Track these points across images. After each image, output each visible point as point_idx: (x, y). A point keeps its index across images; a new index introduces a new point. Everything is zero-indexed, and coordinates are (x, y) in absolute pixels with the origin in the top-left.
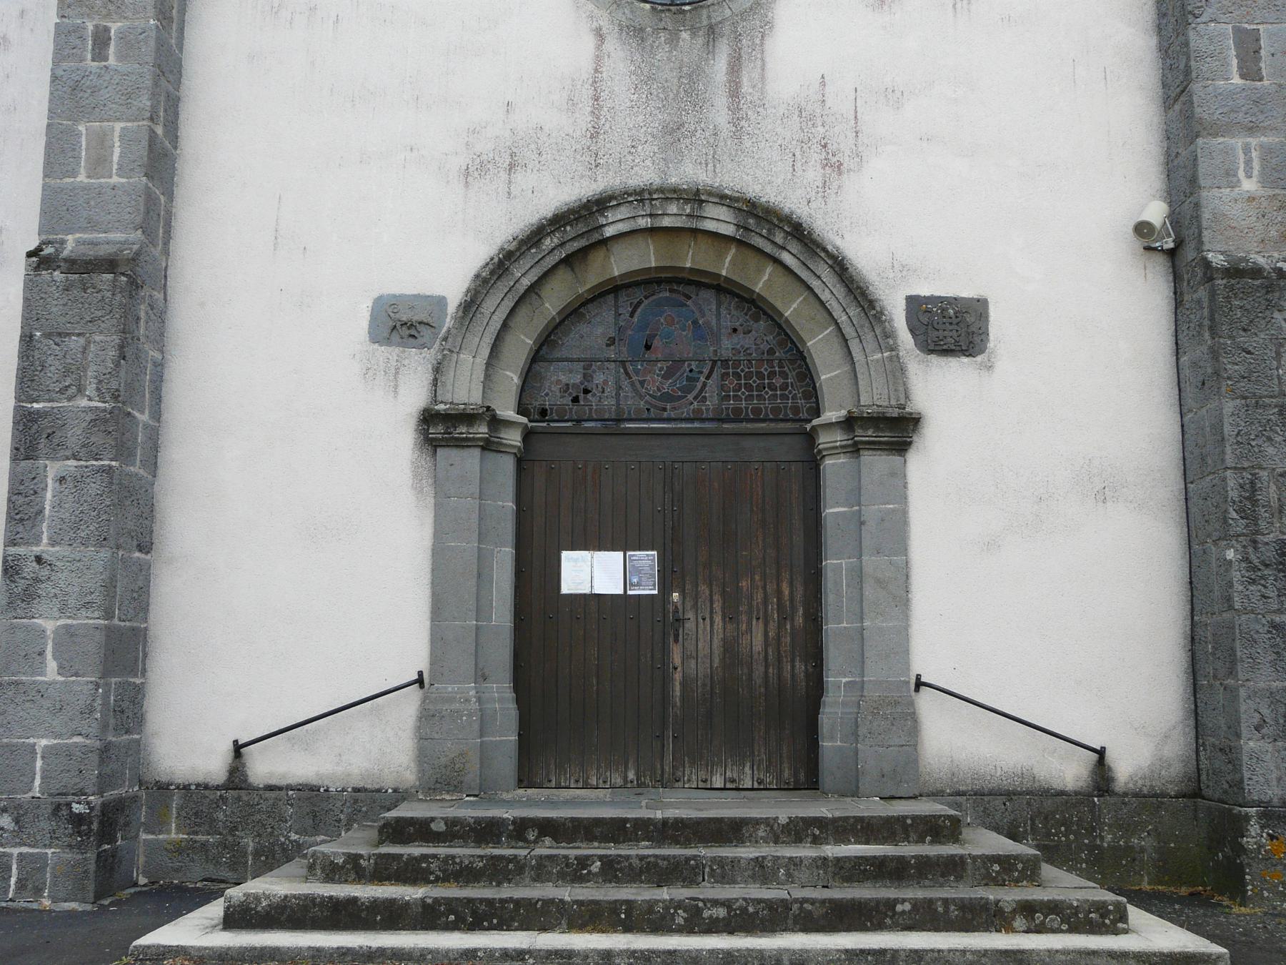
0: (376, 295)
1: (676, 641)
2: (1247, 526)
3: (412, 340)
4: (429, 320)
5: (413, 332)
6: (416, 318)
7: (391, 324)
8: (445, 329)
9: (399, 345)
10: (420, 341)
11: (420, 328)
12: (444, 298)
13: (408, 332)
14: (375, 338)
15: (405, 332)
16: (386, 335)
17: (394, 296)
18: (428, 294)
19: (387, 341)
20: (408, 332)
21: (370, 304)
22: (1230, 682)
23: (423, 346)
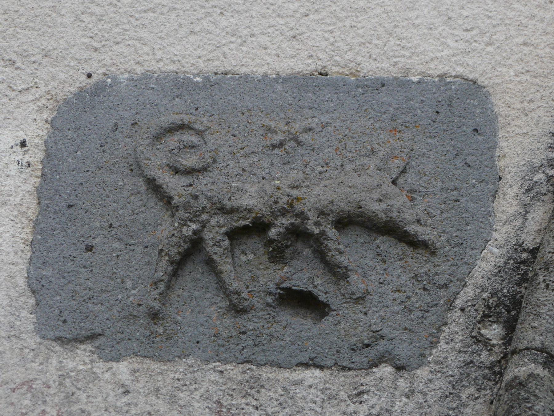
0: (67, 80)
1: (491, 340)
2: (244, 372)
3: (297, 325)
4: (407, 214)
5: (303, 274)
6: (322, 194)
7: (166, 231)
8: (490, 260)
9: (220, 350)
10: (346, 324)
11: (350, 250)
12: (473, 89)
13: (272, 277)
14: (70, 314)
15: (253, 272)
16: (139, 293)
17: (179, 85)
18: (374, 67)
19: (150, 331)
20: (272, 277)
21: (36, 132)
22: (492, 398)
23: (370, 353)
